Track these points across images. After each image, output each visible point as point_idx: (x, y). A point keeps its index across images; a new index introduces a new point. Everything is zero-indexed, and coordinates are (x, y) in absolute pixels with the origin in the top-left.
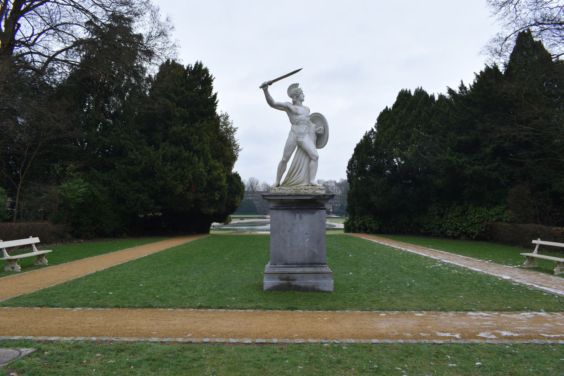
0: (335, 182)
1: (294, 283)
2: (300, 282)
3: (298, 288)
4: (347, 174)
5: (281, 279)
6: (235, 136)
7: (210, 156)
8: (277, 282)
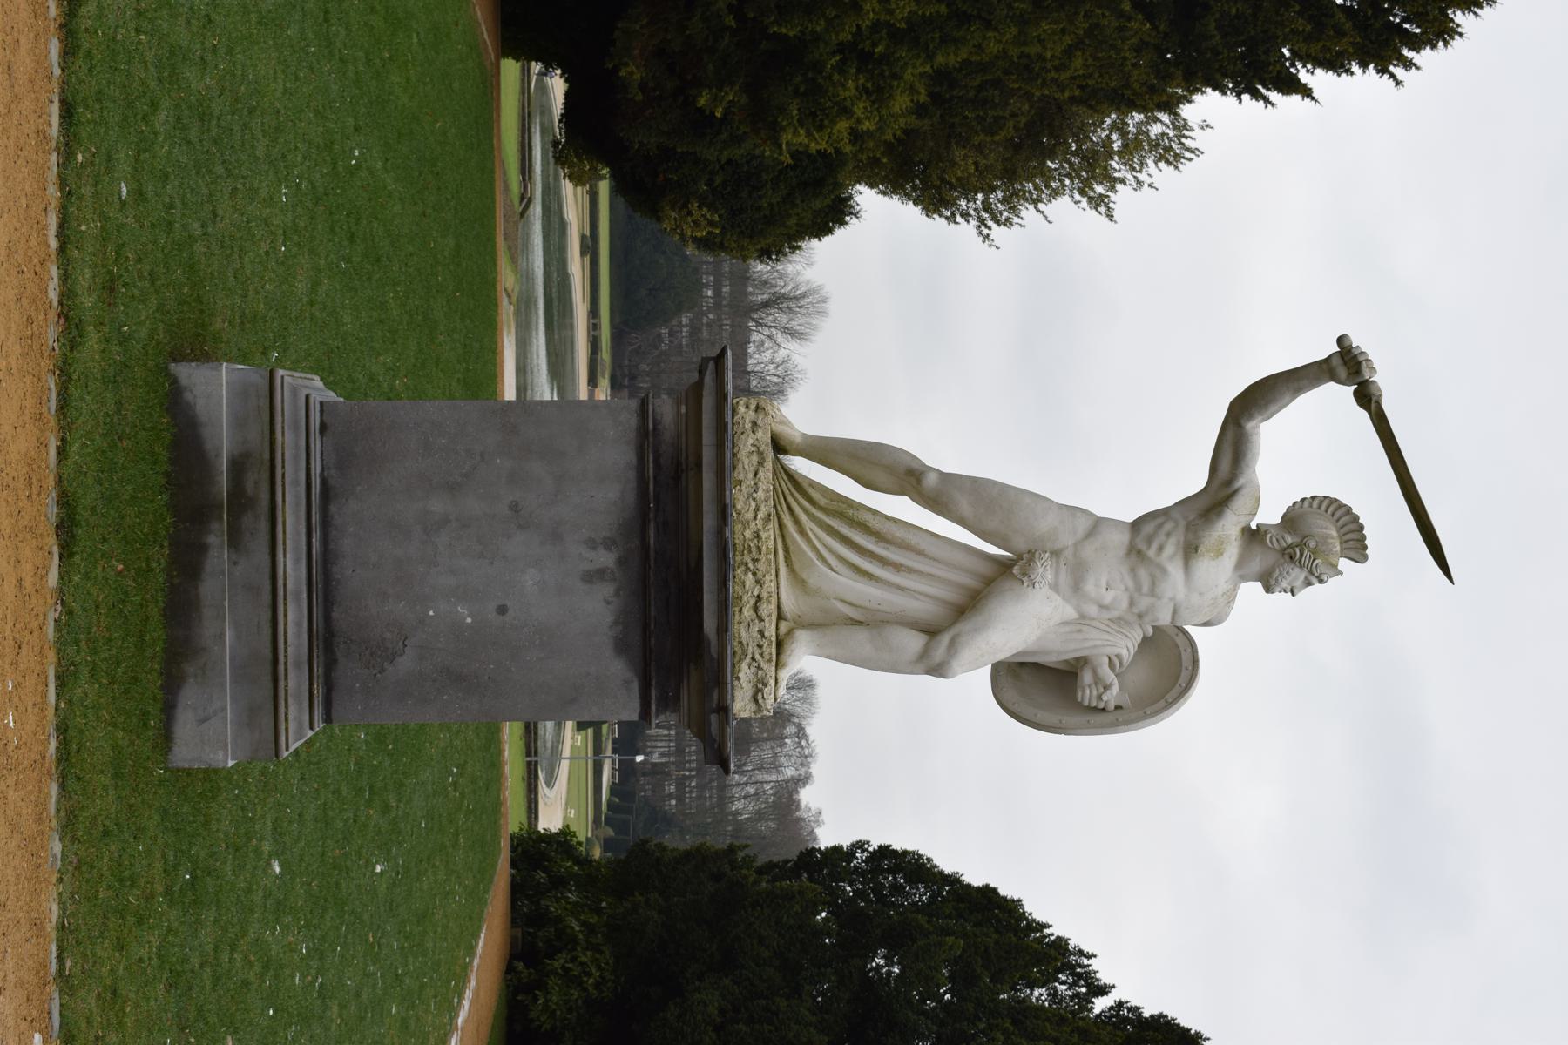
0: (803, 780)
1: (218, 555)
2: (223, 572)
3: (187, 562)
4: (846, 842)
5: (238, 466)
6: (1064, 201)
7: (947, 59)
8: (222, 440)
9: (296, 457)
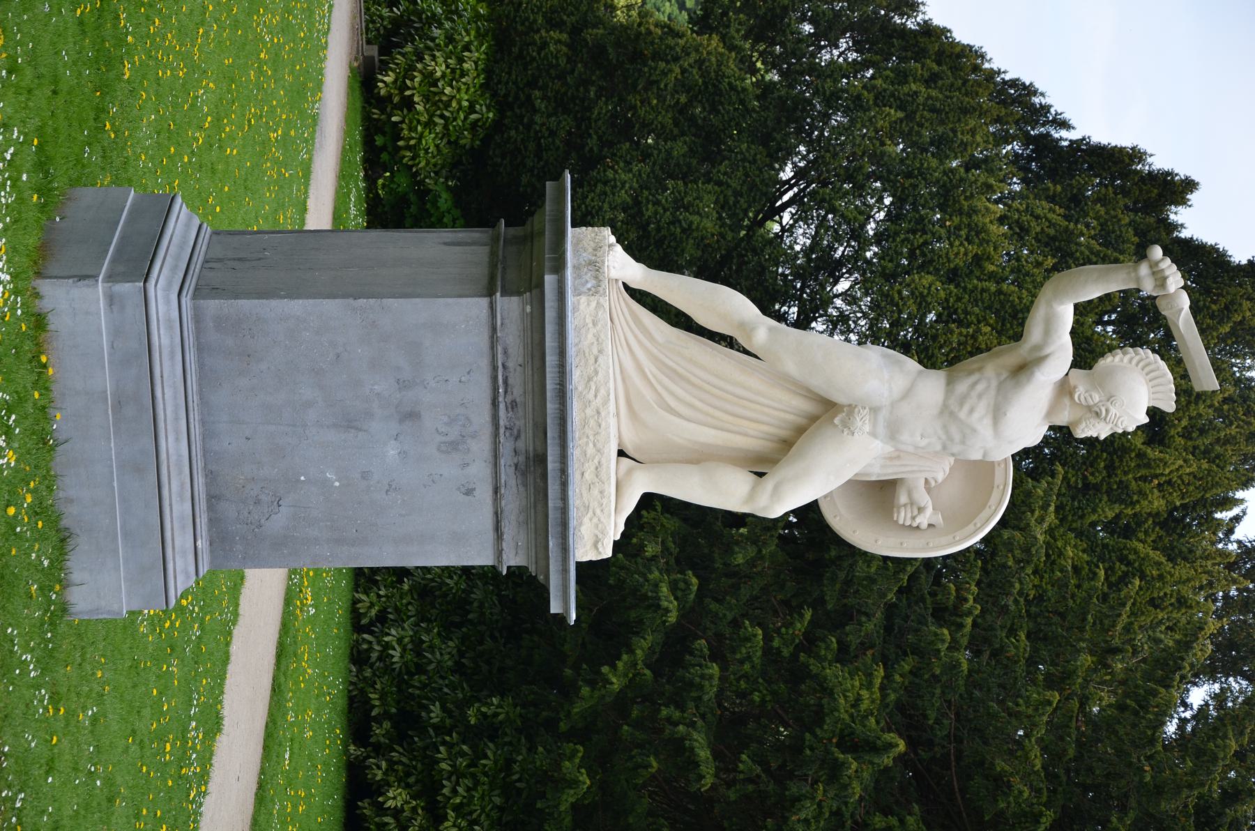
9: (172, 354)
